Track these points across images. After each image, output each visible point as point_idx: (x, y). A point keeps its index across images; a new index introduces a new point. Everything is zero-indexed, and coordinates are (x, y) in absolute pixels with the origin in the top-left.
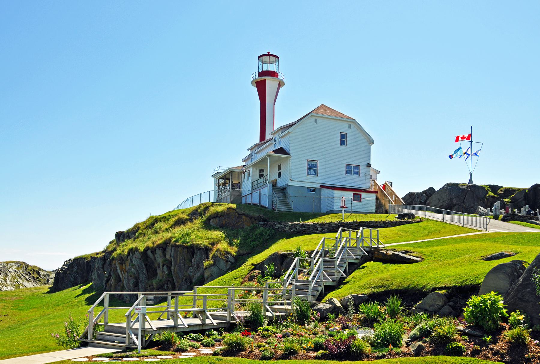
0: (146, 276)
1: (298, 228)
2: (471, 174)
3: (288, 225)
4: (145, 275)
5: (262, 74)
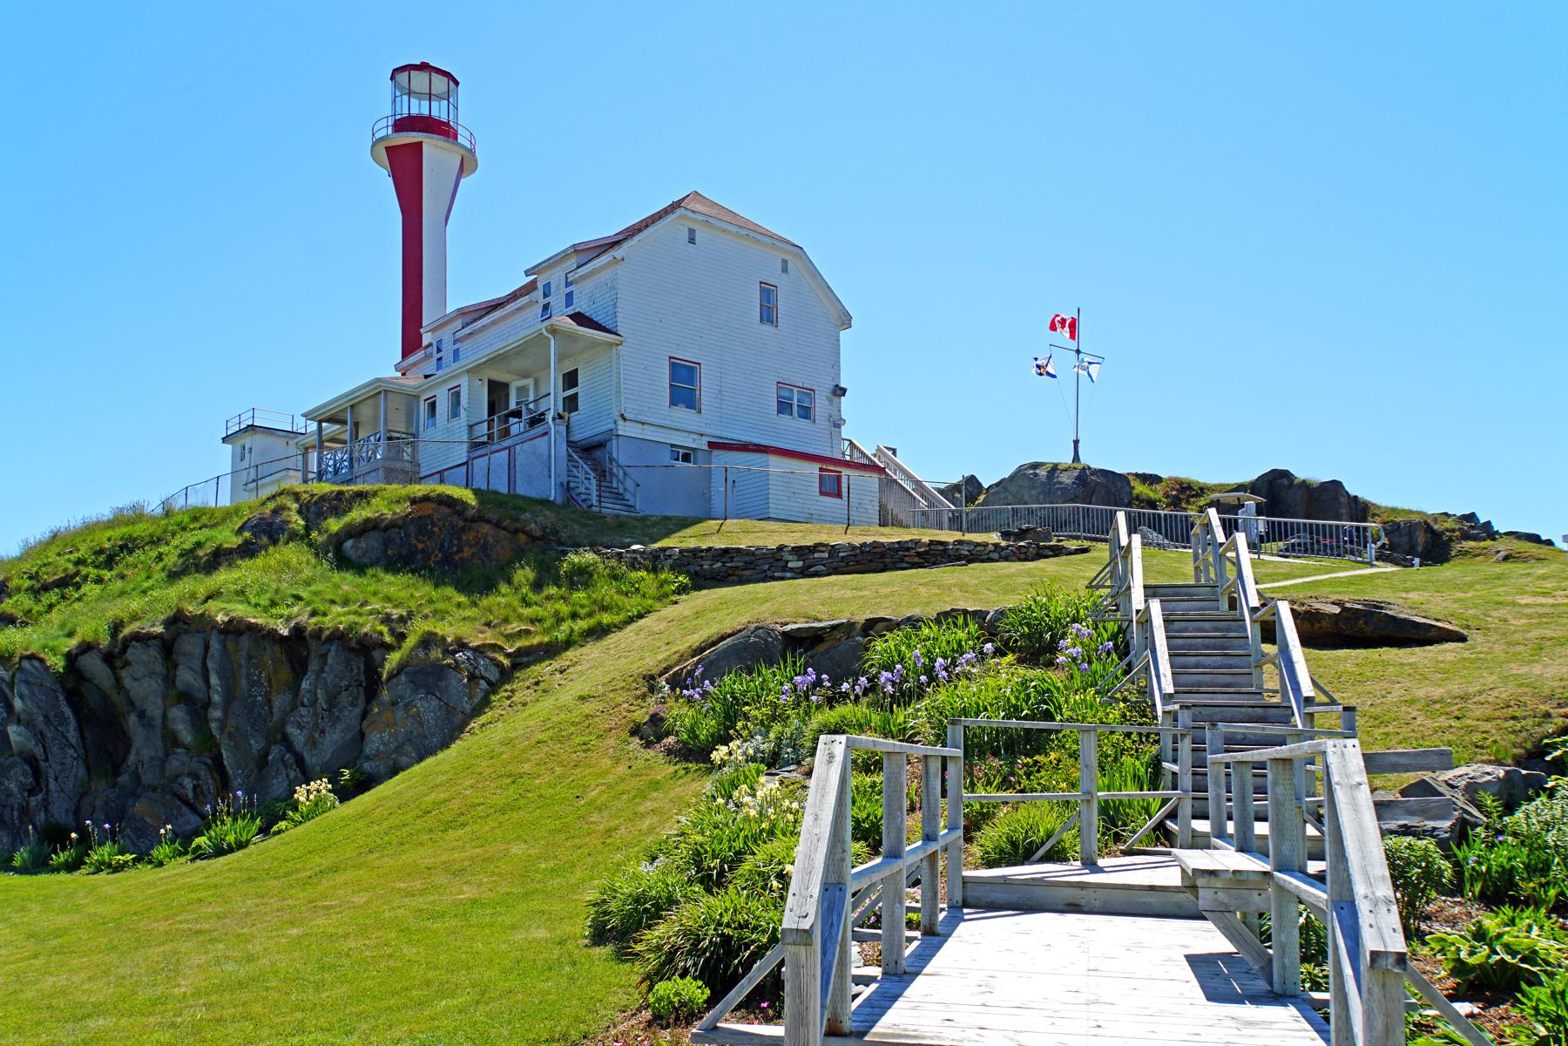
0: (76, 751)
1: (709, 562)
2: (1076, 442)
3: (670, 556)
4: (73, 747)
5: (402, 125)
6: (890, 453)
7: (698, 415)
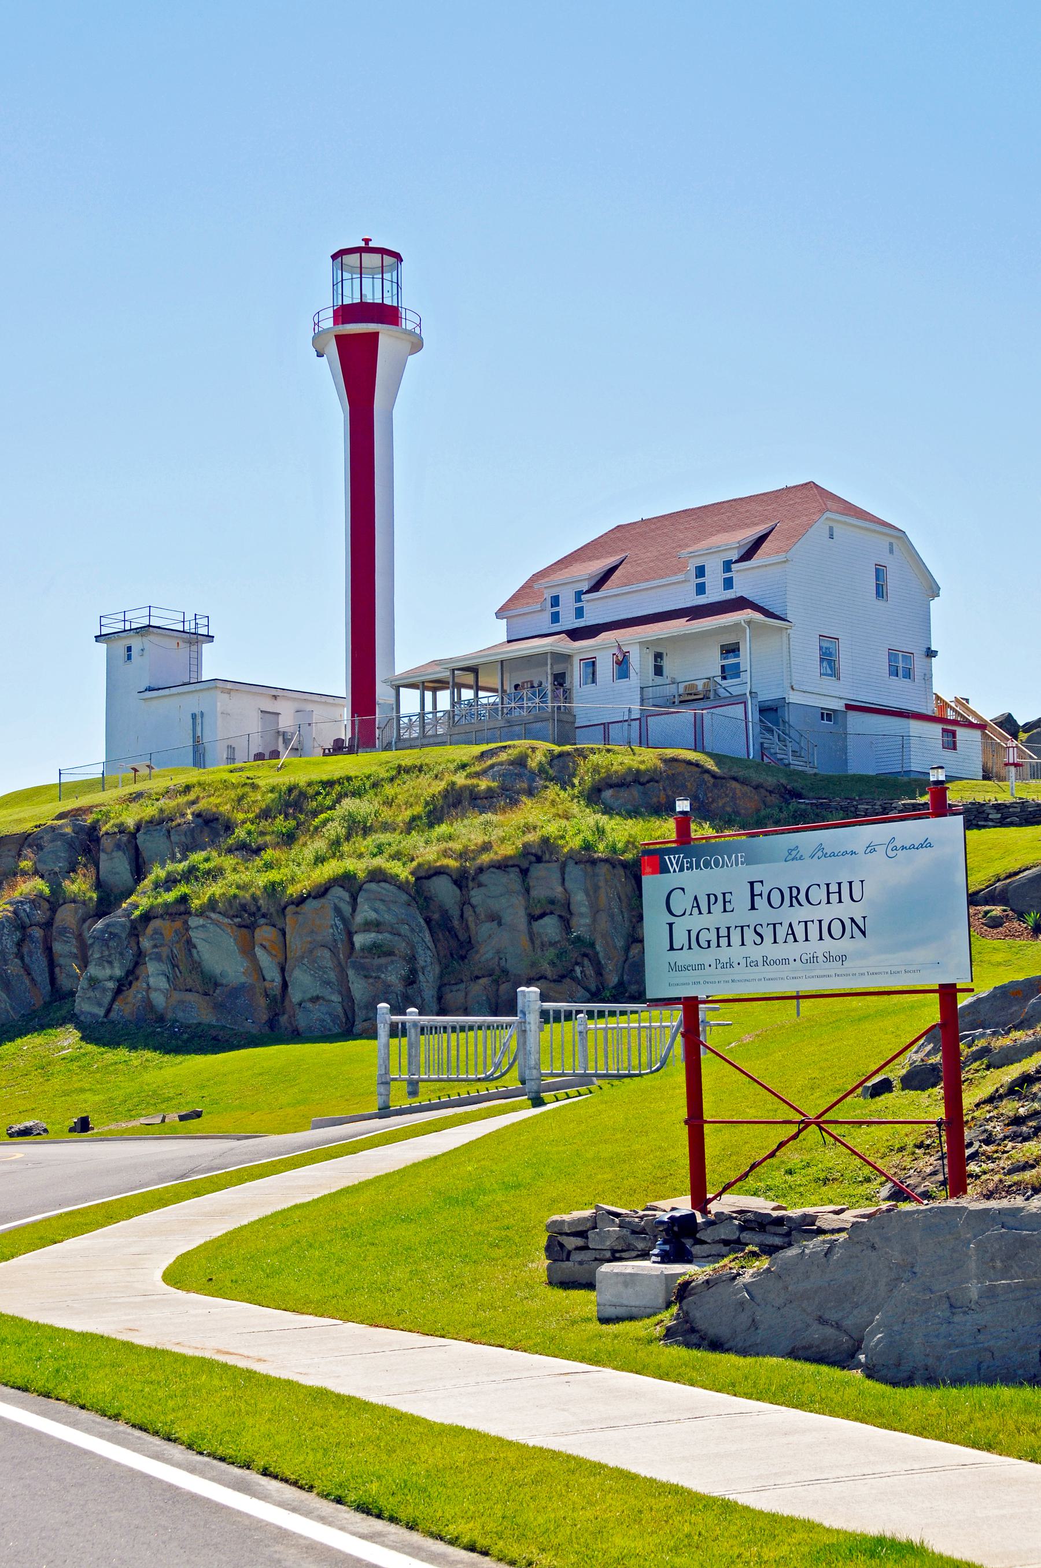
5: (345, 313)
6: (964, 702)
7: (837, 682)
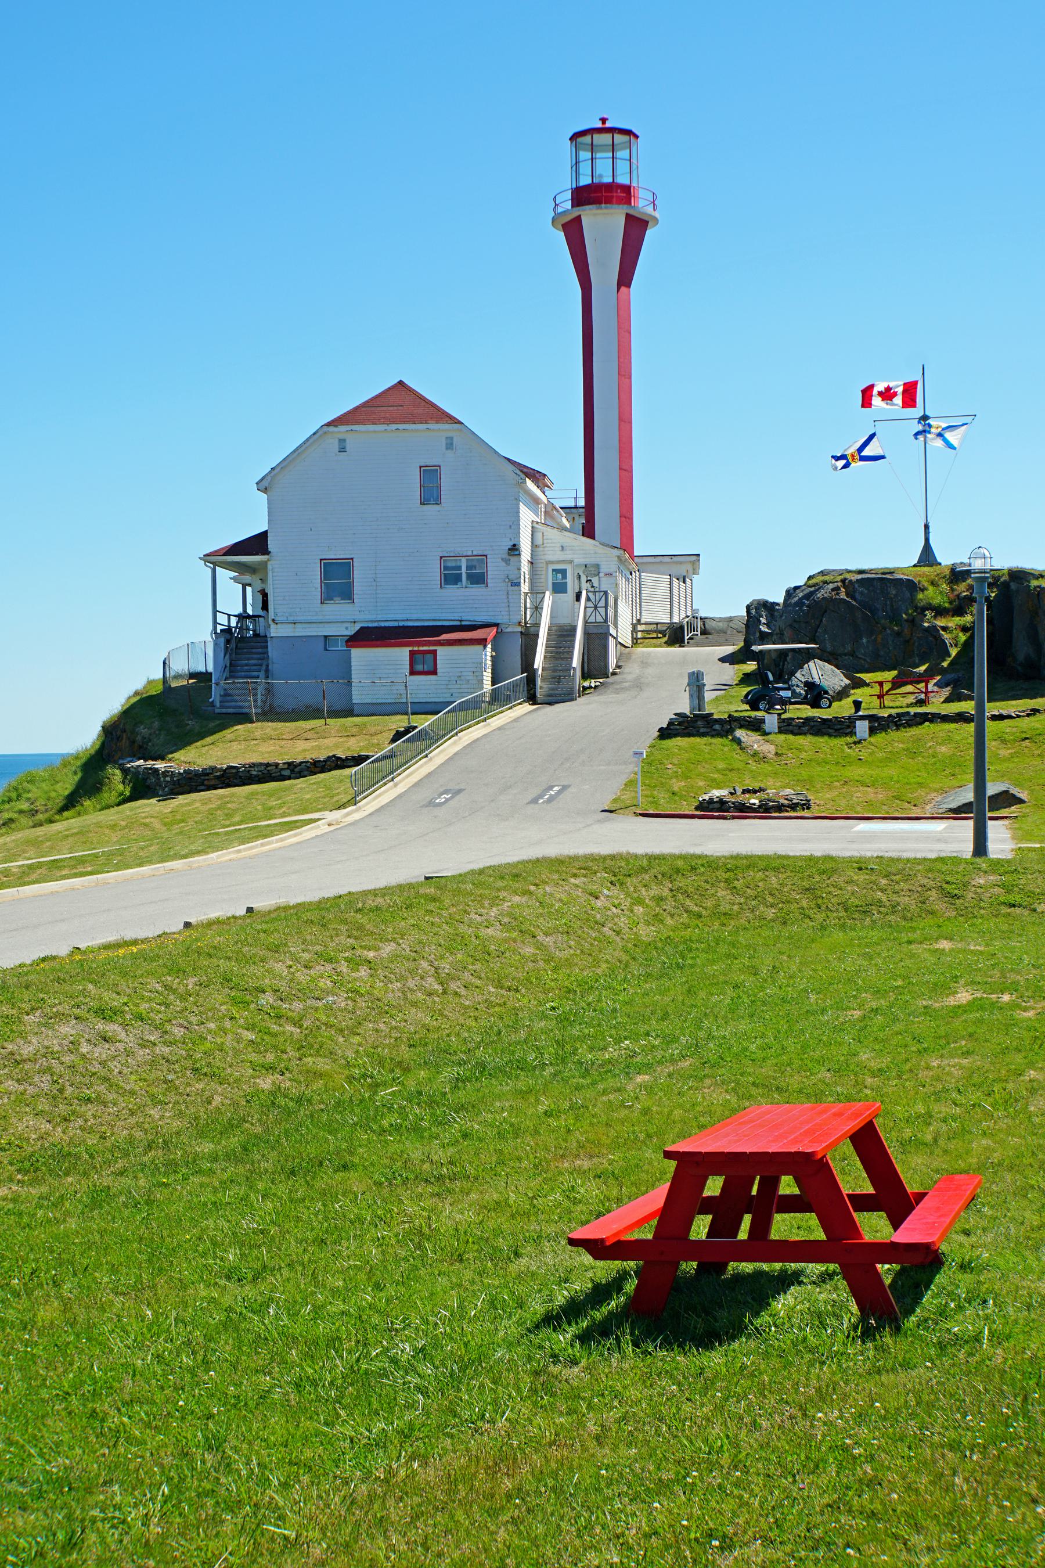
2: (927, 527)
